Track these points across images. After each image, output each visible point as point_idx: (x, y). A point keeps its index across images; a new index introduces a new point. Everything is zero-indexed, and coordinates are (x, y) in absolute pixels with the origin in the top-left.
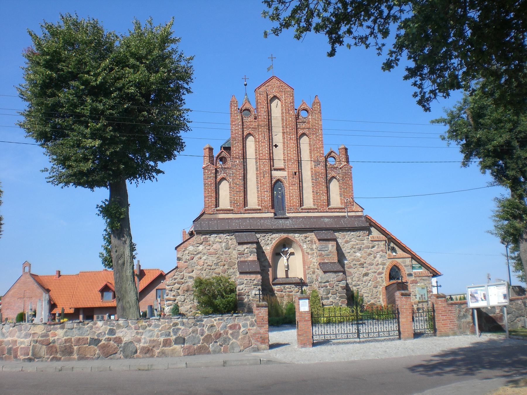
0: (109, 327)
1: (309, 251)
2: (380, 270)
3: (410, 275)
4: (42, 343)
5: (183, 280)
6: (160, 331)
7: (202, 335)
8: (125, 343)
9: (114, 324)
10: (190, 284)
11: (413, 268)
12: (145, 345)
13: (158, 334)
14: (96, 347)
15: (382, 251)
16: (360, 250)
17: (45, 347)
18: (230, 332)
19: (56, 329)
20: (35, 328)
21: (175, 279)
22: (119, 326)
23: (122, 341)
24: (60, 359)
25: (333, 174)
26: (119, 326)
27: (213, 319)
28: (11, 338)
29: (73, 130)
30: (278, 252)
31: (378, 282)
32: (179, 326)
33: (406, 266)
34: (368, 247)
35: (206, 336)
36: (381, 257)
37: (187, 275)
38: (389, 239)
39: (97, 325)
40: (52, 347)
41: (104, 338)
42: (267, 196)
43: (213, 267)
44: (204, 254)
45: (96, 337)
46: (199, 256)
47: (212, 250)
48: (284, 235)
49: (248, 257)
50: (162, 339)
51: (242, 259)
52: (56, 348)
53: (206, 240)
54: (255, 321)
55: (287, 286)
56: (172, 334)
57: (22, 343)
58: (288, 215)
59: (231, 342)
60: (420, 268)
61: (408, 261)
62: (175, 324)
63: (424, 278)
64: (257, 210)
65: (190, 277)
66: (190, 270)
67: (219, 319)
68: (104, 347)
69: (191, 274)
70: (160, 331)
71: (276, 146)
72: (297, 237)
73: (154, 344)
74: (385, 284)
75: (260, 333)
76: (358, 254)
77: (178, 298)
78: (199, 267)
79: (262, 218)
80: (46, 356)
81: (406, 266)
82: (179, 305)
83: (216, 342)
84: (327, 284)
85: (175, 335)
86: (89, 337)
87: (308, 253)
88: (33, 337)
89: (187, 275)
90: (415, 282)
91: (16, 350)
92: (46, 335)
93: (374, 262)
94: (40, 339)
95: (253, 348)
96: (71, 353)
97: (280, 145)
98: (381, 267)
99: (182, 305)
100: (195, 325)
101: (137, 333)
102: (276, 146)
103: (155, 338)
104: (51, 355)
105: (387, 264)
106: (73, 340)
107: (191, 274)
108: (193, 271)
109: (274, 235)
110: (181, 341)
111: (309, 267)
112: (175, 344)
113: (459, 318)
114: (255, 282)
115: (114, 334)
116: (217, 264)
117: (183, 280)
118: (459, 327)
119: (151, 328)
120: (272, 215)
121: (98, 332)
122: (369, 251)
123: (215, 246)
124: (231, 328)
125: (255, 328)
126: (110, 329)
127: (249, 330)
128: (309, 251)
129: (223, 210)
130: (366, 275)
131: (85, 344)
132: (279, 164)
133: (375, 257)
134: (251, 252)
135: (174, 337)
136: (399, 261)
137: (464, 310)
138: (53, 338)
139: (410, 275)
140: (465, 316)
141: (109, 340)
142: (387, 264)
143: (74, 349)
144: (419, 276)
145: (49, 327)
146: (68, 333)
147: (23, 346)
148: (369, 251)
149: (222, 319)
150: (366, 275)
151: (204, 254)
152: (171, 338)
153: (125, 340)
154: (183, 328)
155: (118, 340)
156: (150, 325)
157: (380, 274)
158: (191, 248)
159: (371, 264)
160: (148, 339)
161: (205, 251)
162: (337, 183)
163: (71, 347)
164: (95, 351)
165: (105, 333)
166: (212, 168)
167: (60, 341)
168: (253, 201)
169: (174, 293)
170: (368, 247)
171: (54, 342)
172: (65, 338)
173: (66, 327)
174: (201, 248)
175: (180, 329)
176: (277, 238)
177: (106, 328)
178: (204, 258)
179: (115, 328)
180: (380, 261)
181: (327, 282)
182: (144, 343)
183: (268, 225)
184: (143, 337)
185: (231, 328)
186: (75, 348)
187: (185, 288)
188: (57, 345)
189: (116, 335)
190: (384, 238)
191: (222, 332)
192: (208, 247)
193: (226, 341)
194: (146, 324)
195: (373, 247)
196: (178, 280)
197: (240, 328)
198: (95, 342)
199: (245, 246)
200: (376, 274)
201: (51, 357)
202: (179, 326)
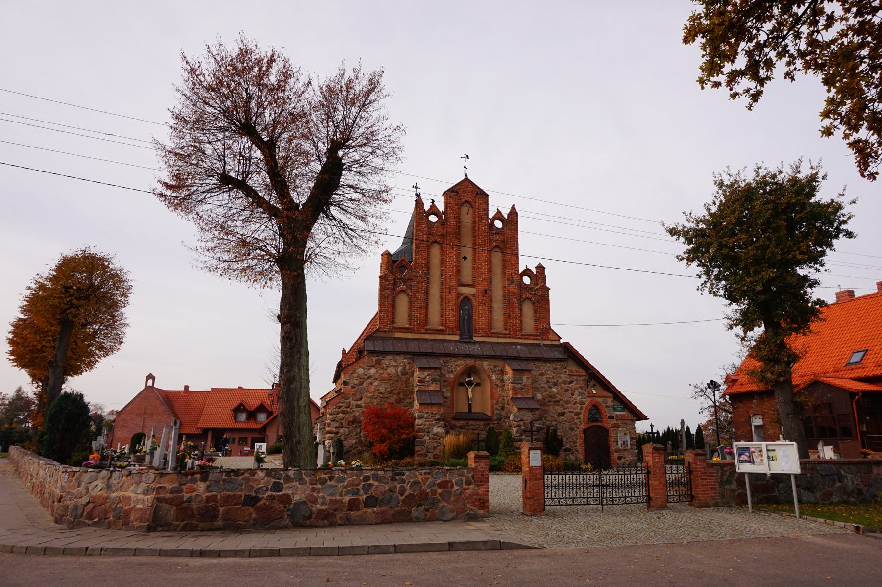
0: (274, 480)
1: (498, 382)
2: (578, 410)
3: (611, 417)
4: (170, 502)
5: (349, 409)
6: (345, 487)
7: (402, 495)
8: (295, 504)
9: (281, 475)
10: (357, 414)
11: (615, 410)
12: (324, 507)
13: (342, 492)
14: (252, 509)
15: (581, 387)
16: (555, 384)
17: (175, 508)
18: (440, 491)
19: (194, 481)
20: (162, 480)
21: (339, 407)
22: (288, 479)
23: (291, 500)
24: (197, 526)
25: (528, 295)
26: (288, 479)
27: (417, 473)
28: (123, 493)
29: (60, 298)
30: (462, 381)
31: (576, 424)
32: (371, 481)
33: (607, 407)
34: (565, 382)
35: (407, 497)
36: (580, 394)
37: (354, 403)
38: (589, 374)
39: (256, 476)
40: (185, 508)
41: (265, 496)
42: (452, 316)
43: (385, 396)
44: (376, 379)
45: (254, 495)
46: (370, 380)
47: (385, 375)
48: (470, 362)
49: (429, 385)
50: (346, 499)
51: (422, 388)
52: (192, 509)
53: (378, 362)
54: (473, 477)
55: (471, 422)
56: (361, 492)
57: (138, 501)
58: (475, 339)
59: (441, 505)
60: (622, 410)
61: (610, 401)
62: (367, 479)
63: (627, 422)
64: (441, 330)
65: (358, 406)
66: (358, 397)
67: (425, 473)
68: (265, 508)
69: (359, 403)
70: (345, 487)
71: (465, 258)
72: (486, 365)
73: (335, 506)
74: (583, 427)
75: (478, 495)
76: (554, 390)
77: (341, 430)
78: (369, 395)
79: (445, 340)
80: (176, 523)
81: (607, 407)
82: (343, 439)
83: (420, 505)
84: (522, 423)
85: (365, 493)
86: (242, 494)
87: (497, 385)
88: (158, 493)
89: (354, 403)
90: (617, 426)
91: (127, 513)
92: (178, 491)
93: (571, 400)
94: (168, 496)
95: (468, 514)
96: (215, 517)
97: (470, 257)
98: (579, 406)
99: (346, 439)
100: (393, 479)
101: (313, 490)
102: (465, 258)
103: (338, 498)
104: (183, 521)
105: (586, 403)
106: (219, 497)
107: (359, 403)
108: (361, 399)
109: (459, 362)
110: (371, 502)
111: (498, 402)
112: (365, 506)
113: (722, 484)
114: (437, 417)
115: (281, 491)
116: (391, 392)
117: (349, 409)
118: (723, 496)
119: (332, 483)
120: (457, 338)
121: (256, 487)
122: (566, 386)
123: (389, 371)
124: (440, 485)
125: (472, 486)
126: (275, 483)
127: (465, 489)
128: (498, 382)
129: (400, 328)
130: (563, 414)
131: (236, 504)
132: (467, 277)
133: (573, 395)
134: (433, 380)
135: (364, 497)
136: (600, 400)
137: (728, 473)
138: (188, 495)
139: (611, 417)
140: (729, 482)
141: (272, 498)
142: (586, 403)
143: (218, 511)
144: (621, 418)
145: (184, 478)
146: (212, 488)
147: (139, 506)
148: (566, 386)
149: (429, 474)
150: (563, 414)
151: (376, 379)
152: (361, 498)
153: (296, 498)
154: (376, 483)
155: (286, 499)
156: (331, 479)
157: (577, 414)
158: (360, 371)
159: (568, 402)
160: (328, 498)
161: (377, 376)
162: (531, 306)
163: (215, 508)
164: (250, 514)
165: (267, 488)
166: (391, 277)
167: (200, 498)
168: (435, 319)
169: (336, 424)
170: (565, 382)
171: (190, 500)
172: (207, 494)
173: (210, 478)
174: (372, 371)
175: (371, 485)
176: (460, 365)
177: (269, 481)
178: (376, 383)
179: (282, 481)
180: (578, 398)
181: (522, 420)
182: (323, 504)
183: (452, 349)
184: (321, 495)
185: (440, 485)
186: (221, 509)
187: (351, 420)
188: (194, 506)
189: (283, 492)
190: (583, 372)
191: (429, 491)
192: (381, 371)
193: (434, 503)
194: (326, 476)
195: (571, 382)
196: (343, 408)
197: (452, 486)
198: (252, 501)
199: (426, 373)
200: (572, 414)
201: (183, 523)
202: (371, 481)
